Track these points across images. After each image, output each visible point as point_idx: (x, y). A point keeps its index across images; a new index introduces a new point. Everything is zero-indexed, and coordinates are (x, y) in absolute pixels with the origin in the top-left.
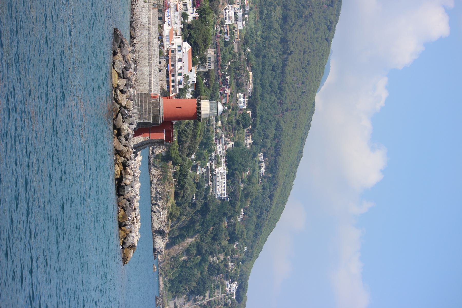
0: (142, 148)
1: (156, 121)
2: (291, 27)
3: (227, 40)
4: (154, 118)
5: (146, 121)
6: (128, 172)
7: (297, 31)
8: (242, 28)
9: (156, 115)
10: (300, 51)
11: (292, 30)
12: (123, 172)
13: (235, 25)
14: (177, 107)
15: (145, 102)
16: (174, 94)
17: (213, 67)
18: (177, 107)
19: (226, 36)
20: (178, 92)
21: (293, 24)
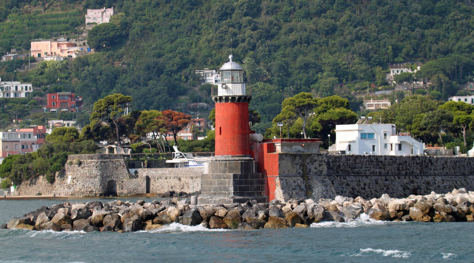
4: (231, 169)
5: (232, 182)
14: (220, 134)
15: (211, 184)
17: (367, 108)
18: (220, 134)
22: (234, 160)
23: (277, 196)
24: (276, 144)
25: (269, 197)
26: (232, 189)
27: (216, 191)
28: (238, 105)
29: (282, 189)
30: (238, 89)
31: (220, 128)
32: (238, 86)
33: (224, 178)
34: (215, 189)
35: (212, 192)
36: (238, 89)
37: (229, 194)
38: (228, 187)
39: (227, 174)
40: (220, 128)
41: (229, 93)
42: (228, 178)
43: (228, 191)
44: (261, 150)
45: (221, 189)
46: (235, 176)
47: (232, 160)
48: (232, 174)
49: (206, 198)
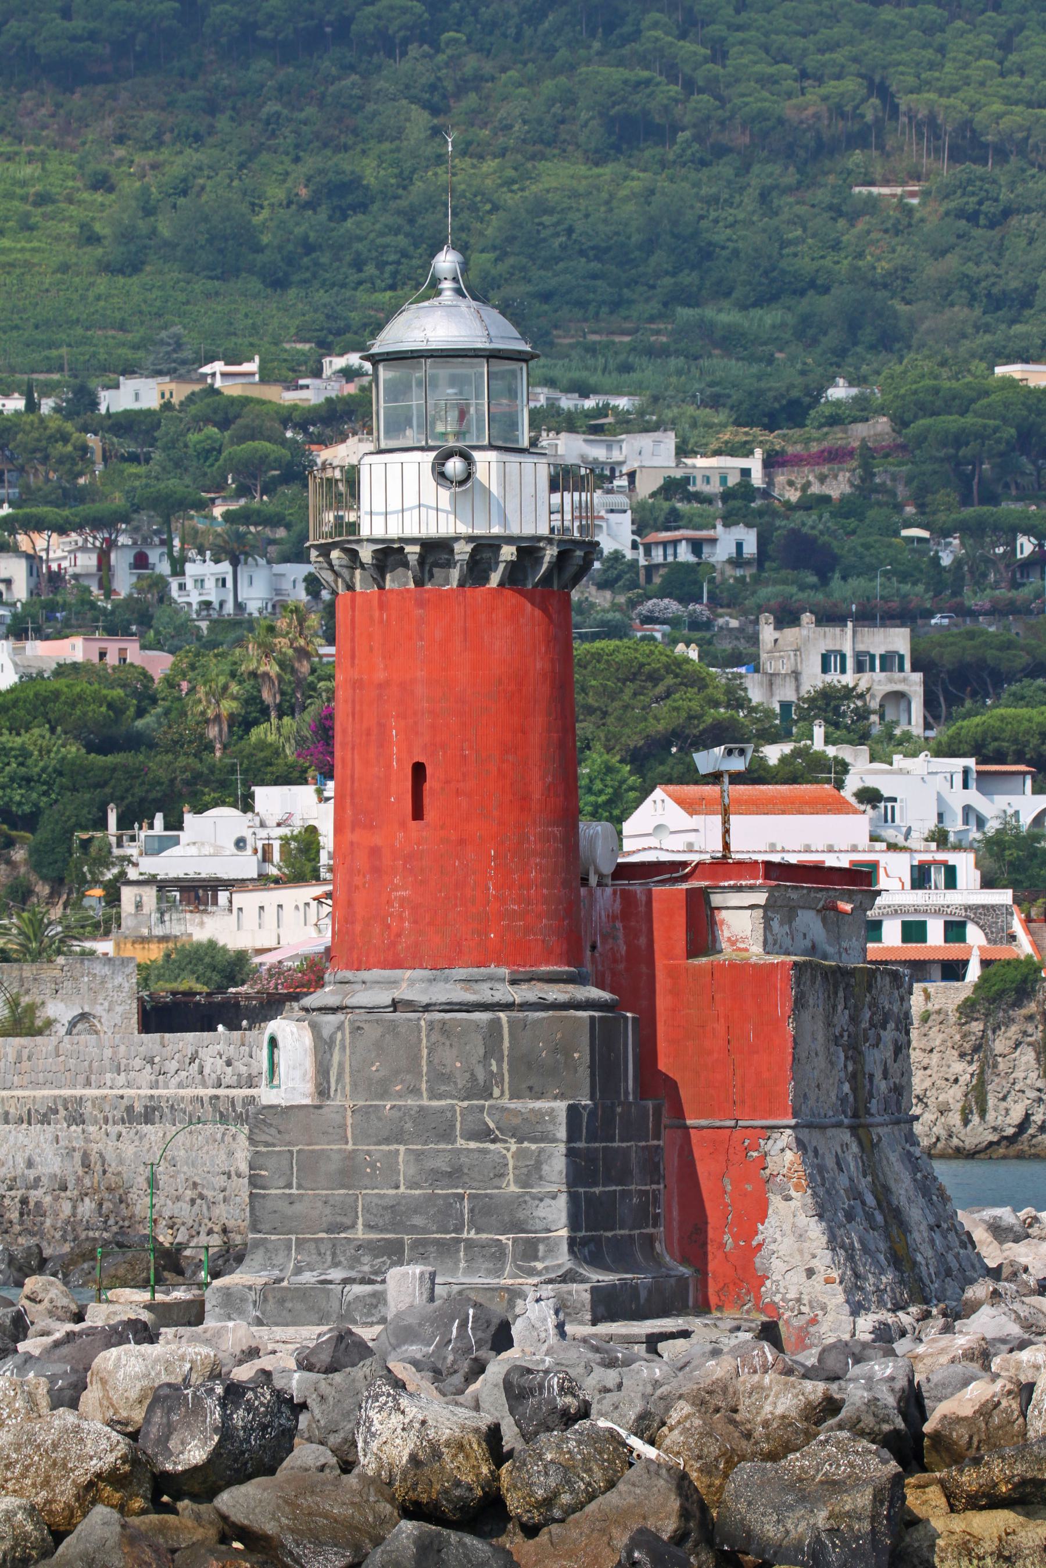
0: (916, 1214)
1: (564, 1049)
2: (690, 86)
3: (751, 548)
4: (531, 1075)
5: (557, 1164)
6: (987, 1410)
7: (719, 53)
8: (669, 441)
9: (492, 1047)
10: (864, 25)
11: (711, 87)
12: (969, 1479)
13: (646, 487)
14: (418, 813)
15: (349, 1173)
16: (1017, 926)
17: (897, 640)
18: (418, 813)
19: (721, 553)
20: (1004, 897)
21: (671, 72)
22: (542, 1005)
23: (777, 1266)
24: (716, 900)
25: (702, 1272)
26: (554, 1215)
27: (396, 1225)
28: (545, 610)
29: (821, 1217)
30: (528, 490)
31: (419, 771)
32: (394, 471)
33: (485, 1134)
34: (395, 1215)
35: (360, 1233)
36: (528, 490)
37: (529, 1251)
38: (519, 1201)
39: (505, 1102)
40: (419, 771)
41: (480, 516)
42: (528, 1130)
43: (516, 1226)
44: (632, 935)
45: (446, 1214)
46: (573, 1112)
47: (525, 1006)
48: (561, 1106)
49: (308, 1277)
